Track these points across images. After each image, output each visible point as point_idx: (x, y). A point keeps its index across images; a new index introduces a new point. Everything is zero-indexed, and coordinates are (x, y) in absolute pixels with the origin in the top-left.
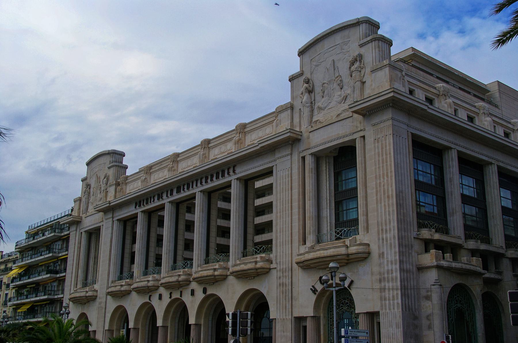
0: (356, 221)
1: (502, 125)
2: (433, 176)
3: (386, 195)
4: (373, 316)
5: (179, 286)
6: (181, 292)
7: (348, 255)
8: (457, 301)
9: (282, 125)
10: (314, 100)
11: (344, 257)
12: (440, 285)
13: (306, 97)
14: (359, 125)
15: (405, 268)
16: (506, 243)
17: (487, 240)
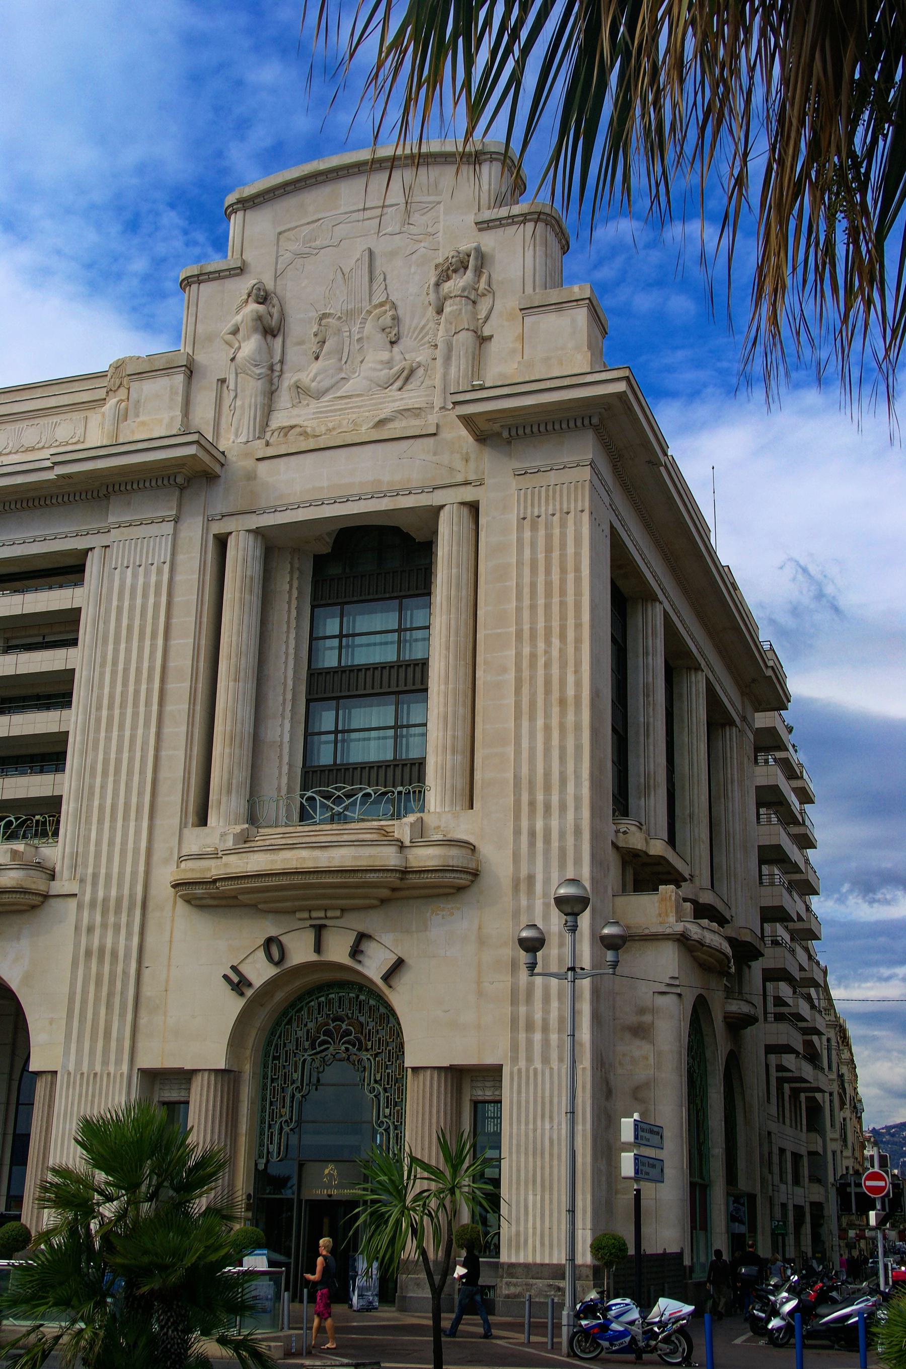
3: (555, 695)
7: (404, 872)
9: (142, 418)
10: (282, 362)
11: (392, 879)
12: (680, 995)
13: (250, 346)
14: (459, 464)
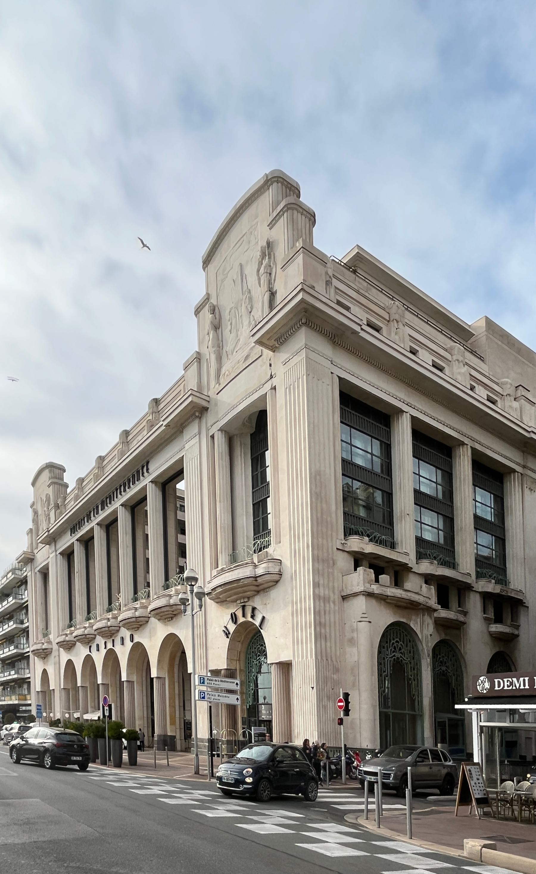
2: (439, 487)
4: (285, 667)
5: (109, 633)
6: (113, 640)
8: (395, 648)
15: (322, 594)
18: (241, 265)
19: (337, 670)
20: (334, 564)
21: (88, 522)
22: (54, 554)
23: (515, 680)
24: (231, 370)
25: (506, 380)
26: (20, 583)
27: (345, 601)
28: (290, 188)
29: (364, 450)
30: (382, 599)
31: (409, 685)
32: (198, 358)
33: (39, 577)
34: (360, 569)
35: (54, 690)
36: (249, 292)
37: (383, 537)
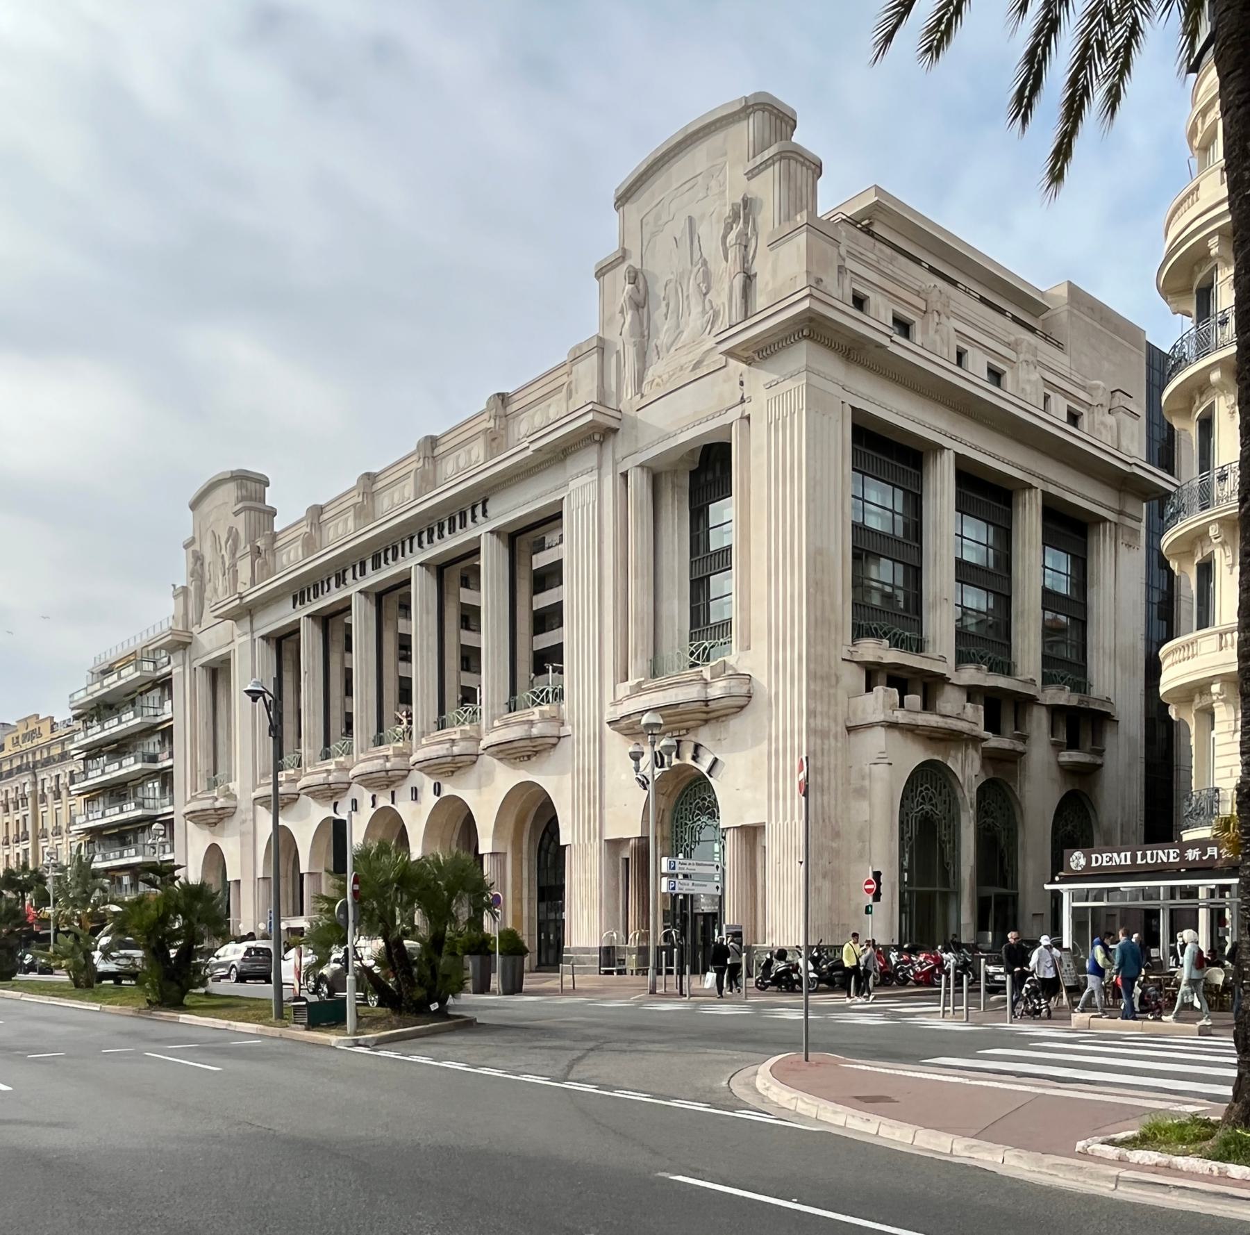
0: (726, 625)
1: (1066, 394)
2: (991, 551)
4: (751, 834)
6: (393, 793)
7: (706, 702)
8: (923, 798)
16: (1043, 674)
17: (1005, 667)
18: (691, 219)
19: (837, 835)
20: (837, 682)
21: (337, 586)
22: (247, 638)
23: (1115, 855)
24: (665, 377)
25: (1098, 382)
26: (149, 685)
27: (852, 734)
28: (780, 120)
29: (881, 506)
30: (910, 730)
31: (942, 851)
32: (601, 347)
33: (202, 679)
34: (879, 690)
35: (238, 882)
36: (705, 263)
37: (907, 634)
